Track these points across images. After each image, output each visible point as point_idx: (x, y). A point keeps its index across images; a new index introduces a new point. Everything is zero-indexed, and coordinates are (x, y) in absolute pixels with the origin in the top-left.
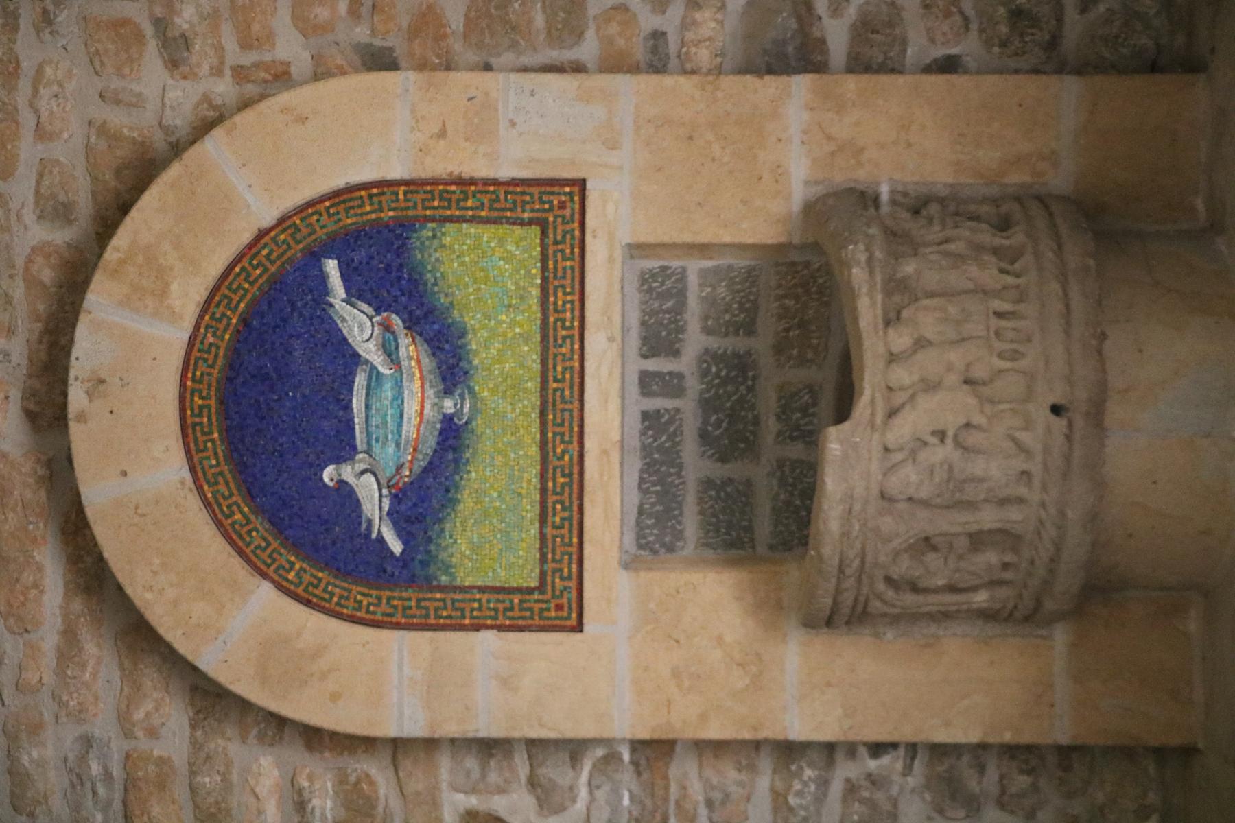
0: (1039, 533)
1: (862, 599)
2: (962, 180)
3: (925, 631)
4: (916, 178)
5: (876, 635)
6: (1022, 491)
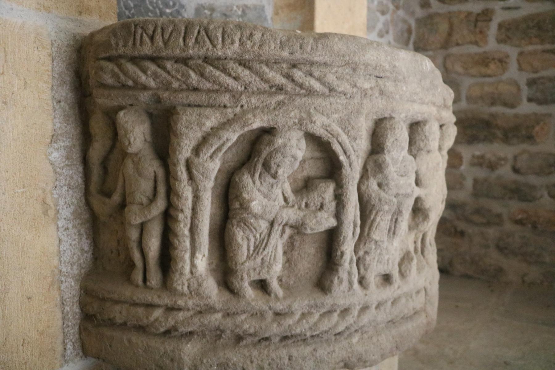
0: (330, 312)
1: (225, 99)
3: (62, 202)
5: (54, 139)
6: (372, 278)
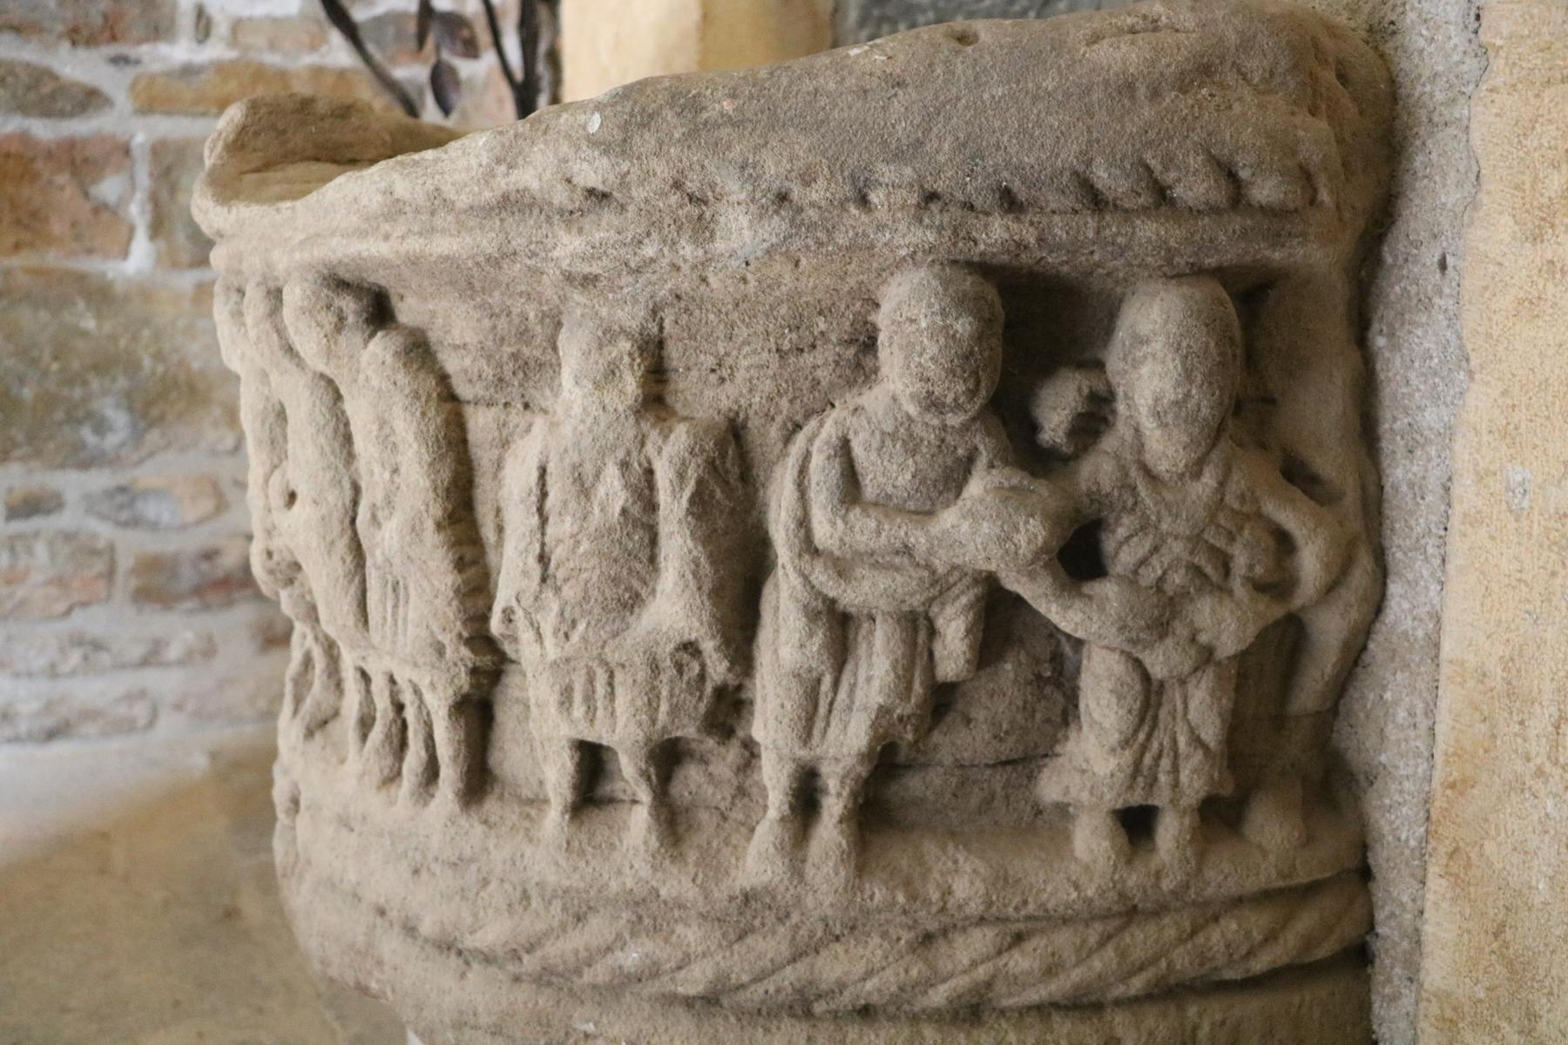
2: (1450, 697)
4: (1466, 495)
